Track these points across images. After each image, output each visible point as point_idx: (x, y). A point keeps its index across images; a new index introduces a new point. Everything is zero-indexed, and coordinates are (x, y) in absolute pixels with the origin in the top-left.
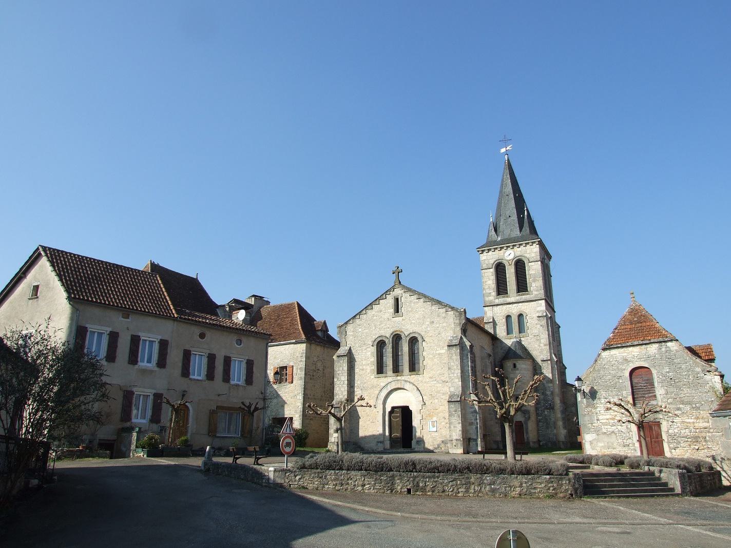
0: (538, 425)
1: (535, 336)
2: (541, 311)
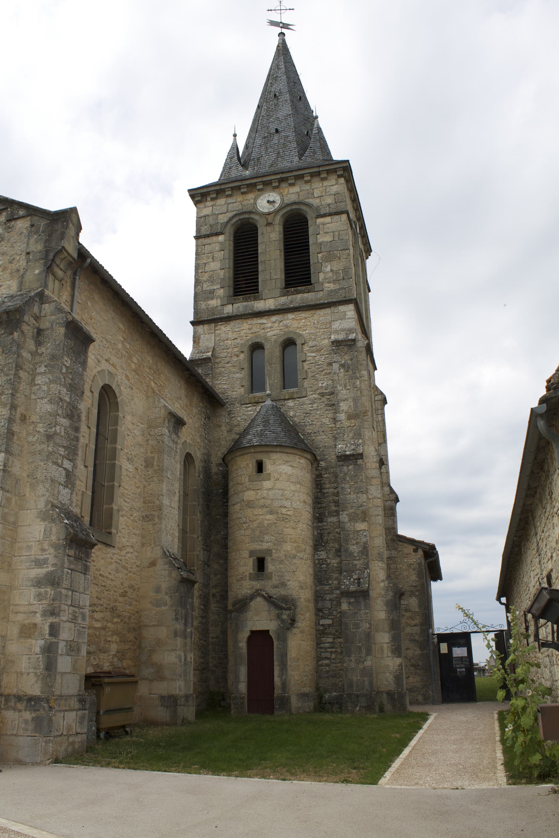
0: (318, 644)
1: (322, 395)
2: (343, 330)
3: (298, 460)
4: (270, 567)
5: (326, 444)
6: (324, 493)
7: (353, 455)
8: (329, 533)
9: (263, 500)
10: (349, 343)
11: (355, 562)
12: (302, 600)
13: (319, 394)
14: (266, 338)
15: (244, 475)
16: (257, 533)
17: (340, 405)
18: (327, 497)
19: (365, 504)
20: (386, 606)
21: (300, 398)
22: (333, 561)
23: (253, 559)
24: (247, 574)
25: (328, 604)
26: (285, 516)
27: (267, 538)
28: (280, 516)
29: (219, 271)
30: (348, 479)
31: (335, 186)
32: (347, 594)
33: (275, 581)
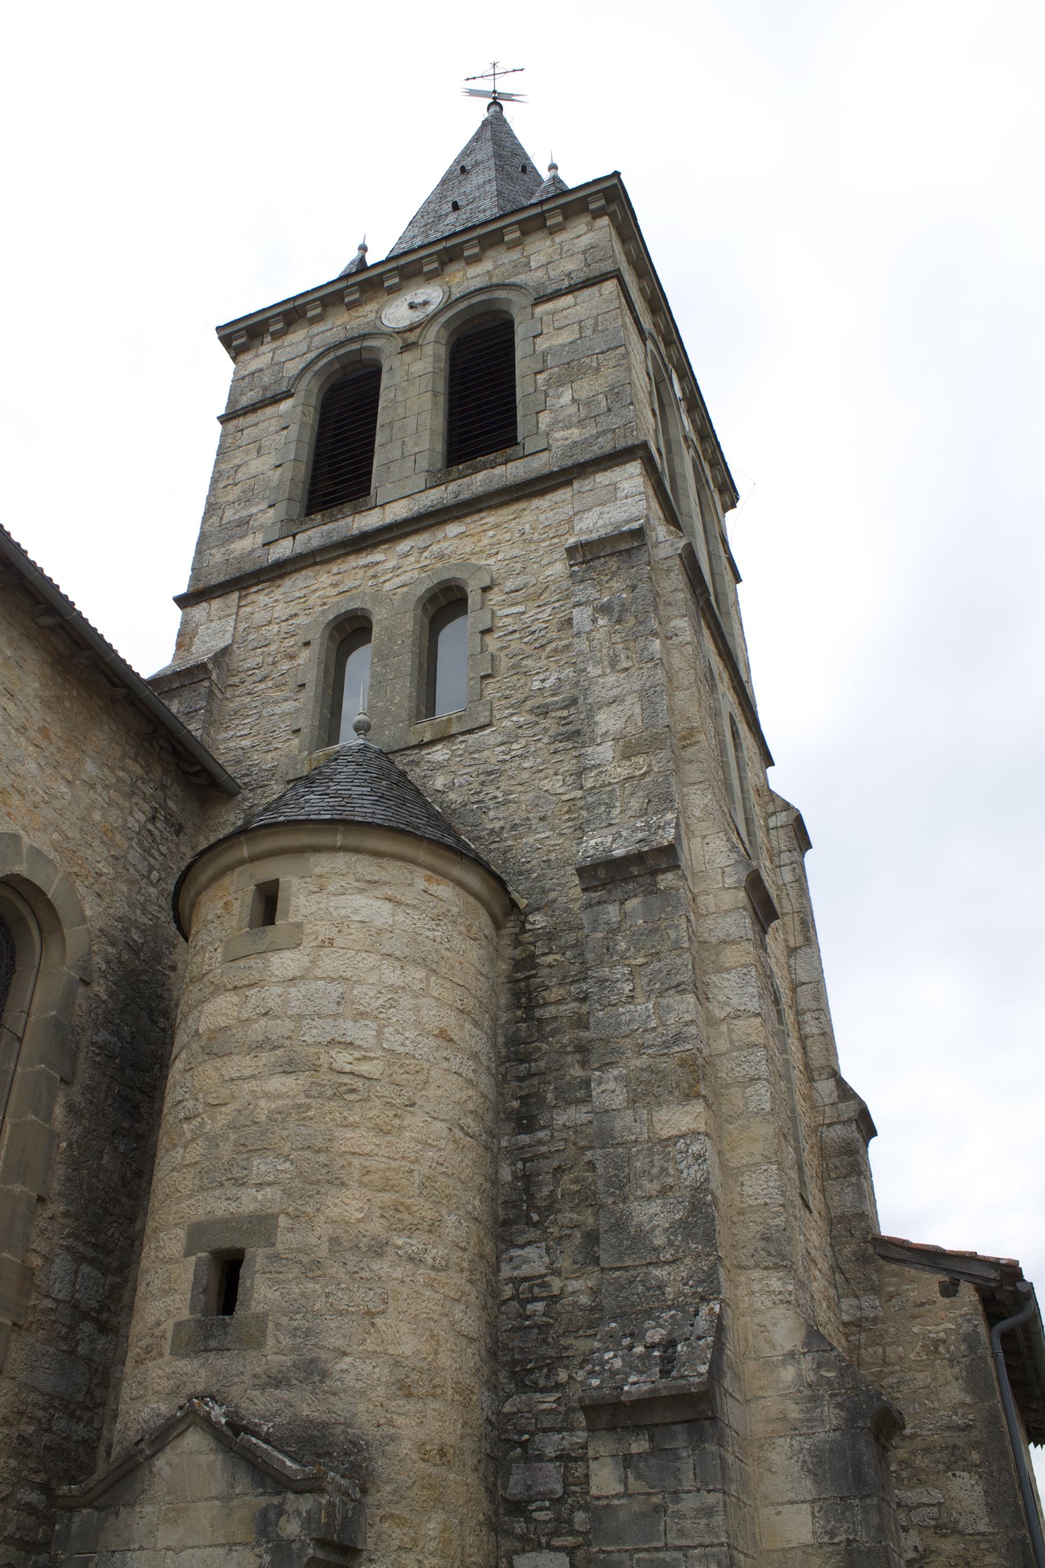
1: (543, 711)
3: (421, 884)
4: (260, 1291)
5: (553, 856)
6: (540, 1021)
7: (638, 858)
8: (559, 1170)
9: (263, 1022)
10: (624, 546)
11: (657, 1272)
12: (405, 1448)
13: (531, 711)
14: (378, 598)
15: (212, 943)
16: (226, 1150)
17: (598, 718)
18: (554, 1033)
19: (693, 1030)
20: (815, 1476)
21: (471, 731)
22: (574, 1285)
23: (199, 1260)
24: (169, 1326)
25: (550, 1478)
26: (346, 1079)
27: (260, 1166)
28: (325, 1077)
29: (270, 473)
30: (623, 945)
31: (589, 235)
32: (612, 1414)
33: (274, 1354)
